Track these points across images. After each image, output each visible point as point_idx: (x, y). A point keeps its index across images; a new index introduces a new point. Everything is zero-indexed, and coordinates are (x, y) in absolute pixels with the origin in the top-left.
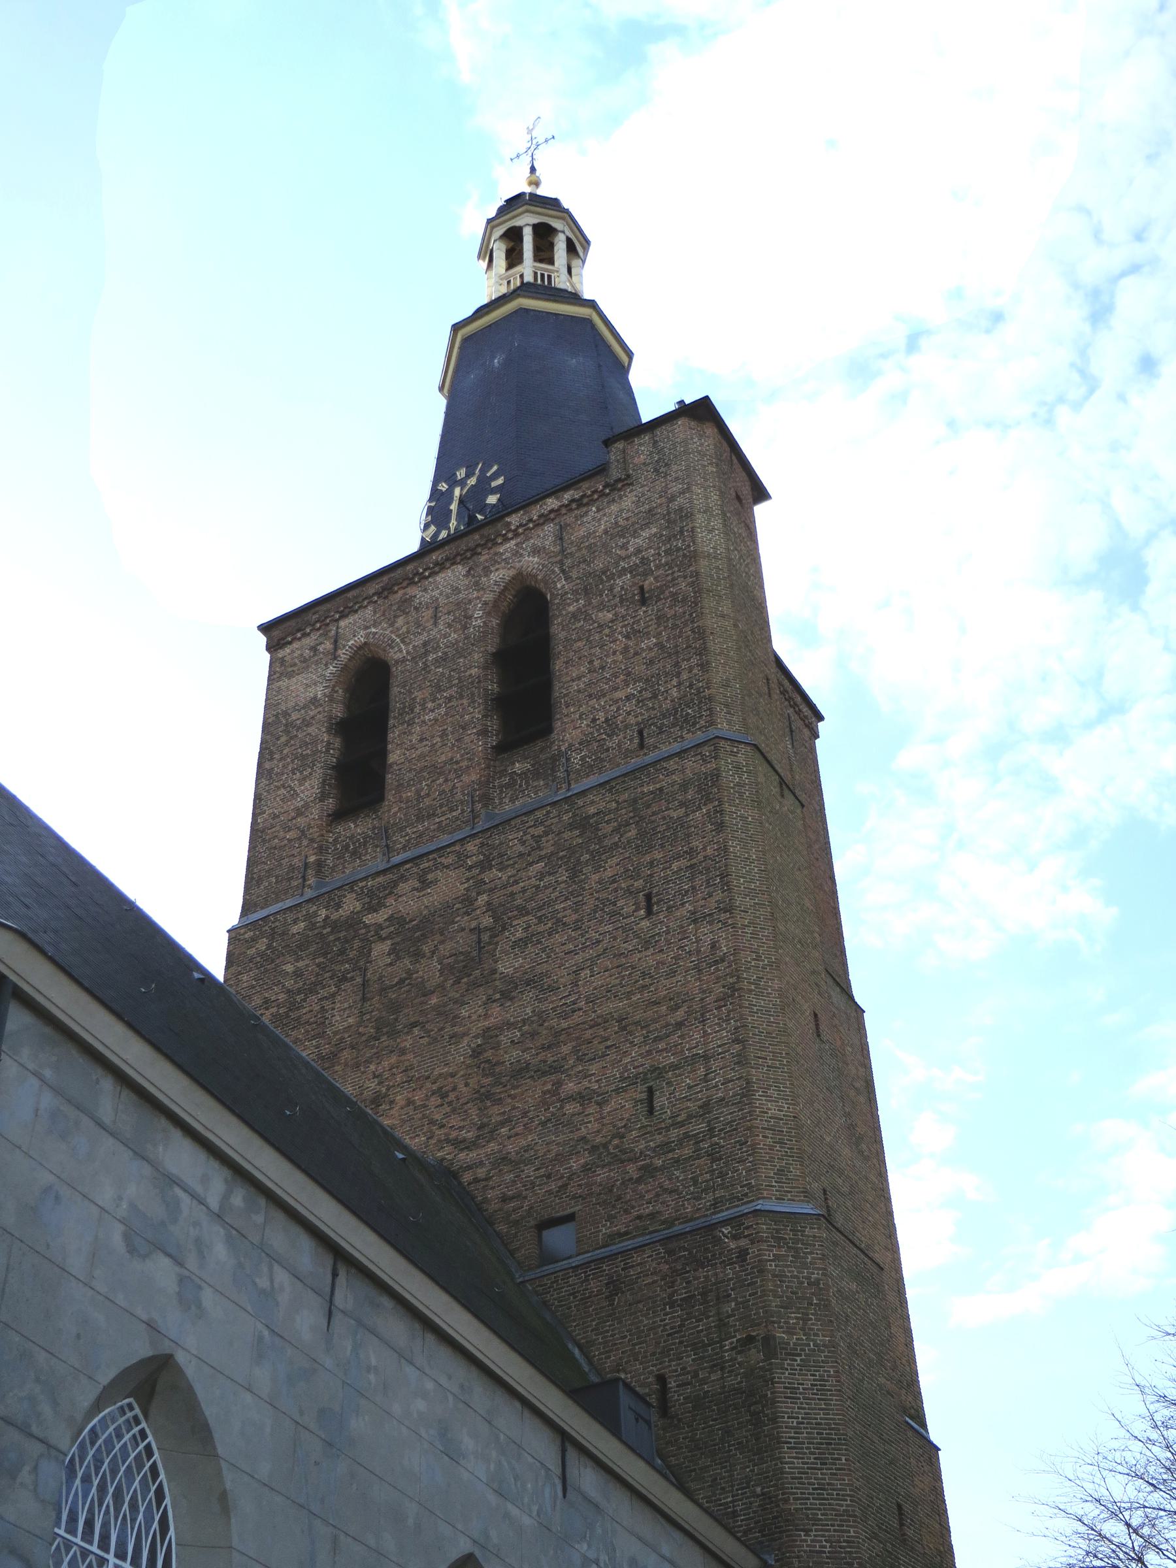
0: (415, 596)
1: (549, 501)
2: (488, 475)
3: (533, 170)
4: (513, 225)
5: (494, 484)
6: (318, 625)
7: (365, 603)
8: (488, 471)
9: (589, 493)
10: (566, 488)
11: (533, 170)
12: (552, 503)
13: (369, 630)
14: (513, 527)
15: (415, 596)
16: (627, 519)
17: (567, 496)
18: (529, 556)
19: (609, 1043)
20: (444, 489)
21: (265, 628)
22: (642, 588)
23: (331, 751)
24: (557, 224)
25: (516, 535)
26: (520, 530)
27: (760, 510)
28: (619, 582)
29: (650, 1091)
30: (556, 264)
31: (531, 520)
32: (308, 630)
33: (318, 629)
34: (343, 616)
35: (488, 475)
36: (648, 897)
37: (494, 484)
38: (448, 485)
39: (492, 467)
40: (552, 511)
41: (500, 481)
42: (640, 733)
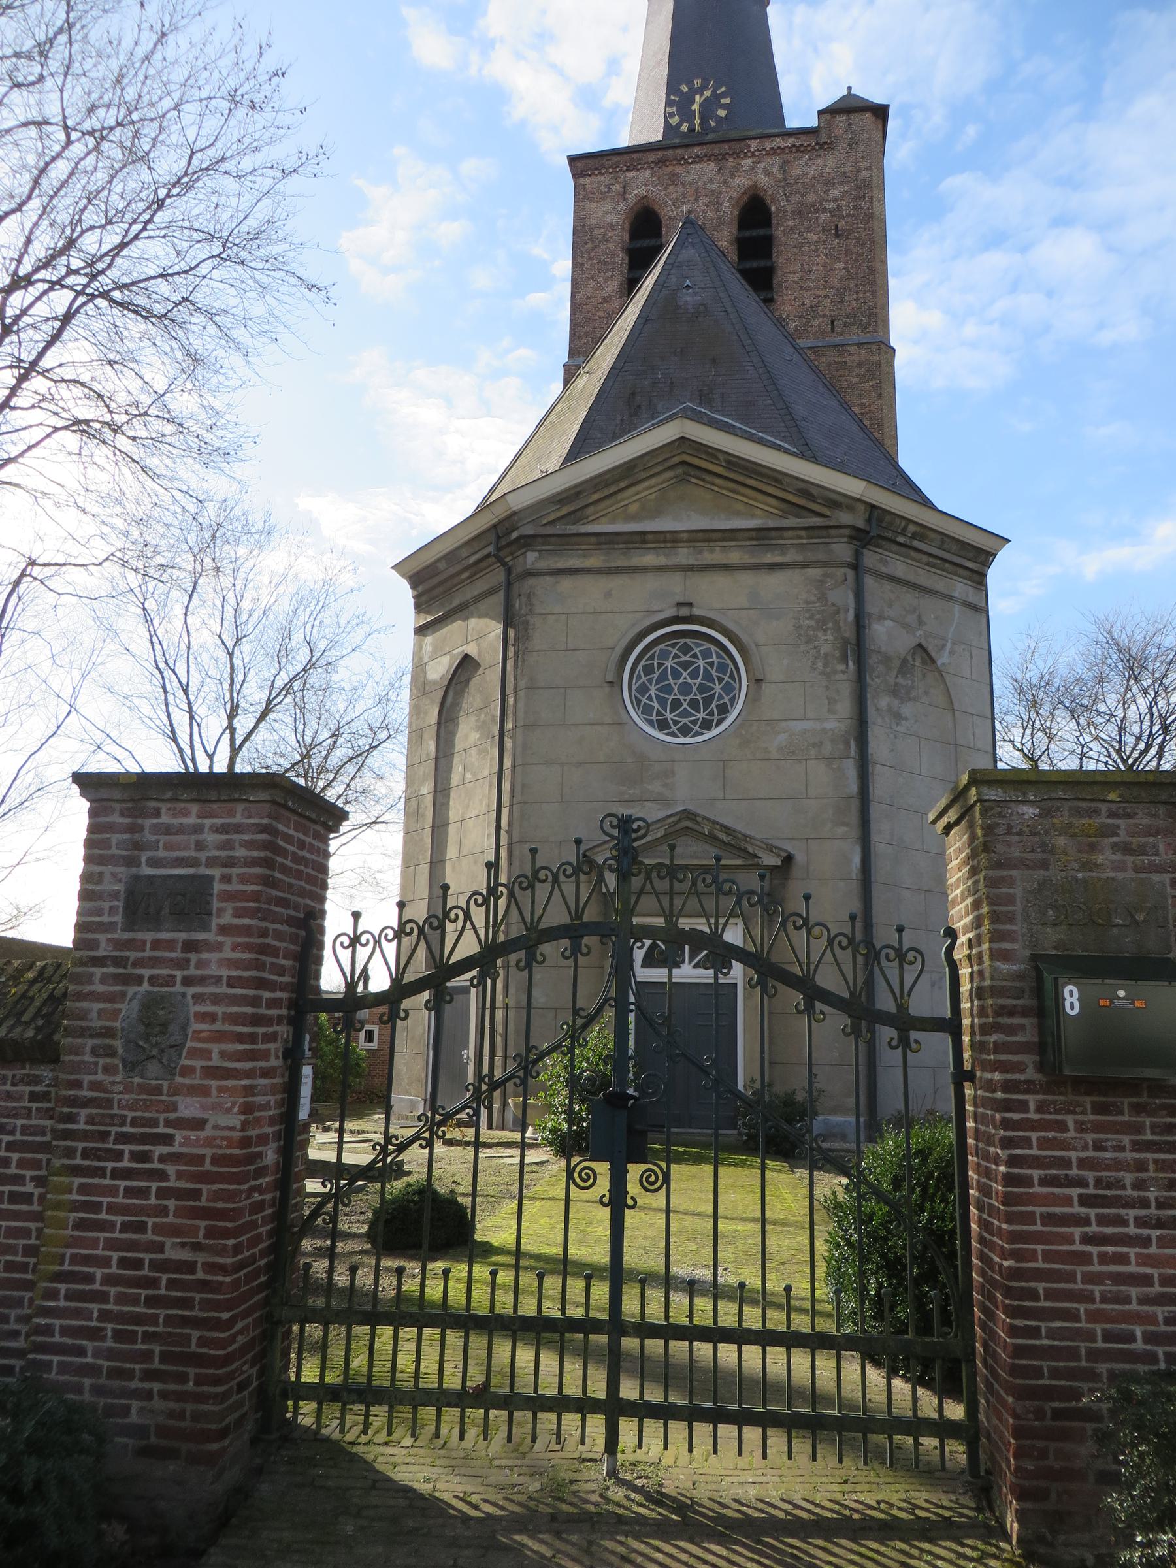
5: (722, 101)
22: (836, 226)
25: (753, 156)
37: (722, 101)
41: (727, 101)
42: (832, 322)
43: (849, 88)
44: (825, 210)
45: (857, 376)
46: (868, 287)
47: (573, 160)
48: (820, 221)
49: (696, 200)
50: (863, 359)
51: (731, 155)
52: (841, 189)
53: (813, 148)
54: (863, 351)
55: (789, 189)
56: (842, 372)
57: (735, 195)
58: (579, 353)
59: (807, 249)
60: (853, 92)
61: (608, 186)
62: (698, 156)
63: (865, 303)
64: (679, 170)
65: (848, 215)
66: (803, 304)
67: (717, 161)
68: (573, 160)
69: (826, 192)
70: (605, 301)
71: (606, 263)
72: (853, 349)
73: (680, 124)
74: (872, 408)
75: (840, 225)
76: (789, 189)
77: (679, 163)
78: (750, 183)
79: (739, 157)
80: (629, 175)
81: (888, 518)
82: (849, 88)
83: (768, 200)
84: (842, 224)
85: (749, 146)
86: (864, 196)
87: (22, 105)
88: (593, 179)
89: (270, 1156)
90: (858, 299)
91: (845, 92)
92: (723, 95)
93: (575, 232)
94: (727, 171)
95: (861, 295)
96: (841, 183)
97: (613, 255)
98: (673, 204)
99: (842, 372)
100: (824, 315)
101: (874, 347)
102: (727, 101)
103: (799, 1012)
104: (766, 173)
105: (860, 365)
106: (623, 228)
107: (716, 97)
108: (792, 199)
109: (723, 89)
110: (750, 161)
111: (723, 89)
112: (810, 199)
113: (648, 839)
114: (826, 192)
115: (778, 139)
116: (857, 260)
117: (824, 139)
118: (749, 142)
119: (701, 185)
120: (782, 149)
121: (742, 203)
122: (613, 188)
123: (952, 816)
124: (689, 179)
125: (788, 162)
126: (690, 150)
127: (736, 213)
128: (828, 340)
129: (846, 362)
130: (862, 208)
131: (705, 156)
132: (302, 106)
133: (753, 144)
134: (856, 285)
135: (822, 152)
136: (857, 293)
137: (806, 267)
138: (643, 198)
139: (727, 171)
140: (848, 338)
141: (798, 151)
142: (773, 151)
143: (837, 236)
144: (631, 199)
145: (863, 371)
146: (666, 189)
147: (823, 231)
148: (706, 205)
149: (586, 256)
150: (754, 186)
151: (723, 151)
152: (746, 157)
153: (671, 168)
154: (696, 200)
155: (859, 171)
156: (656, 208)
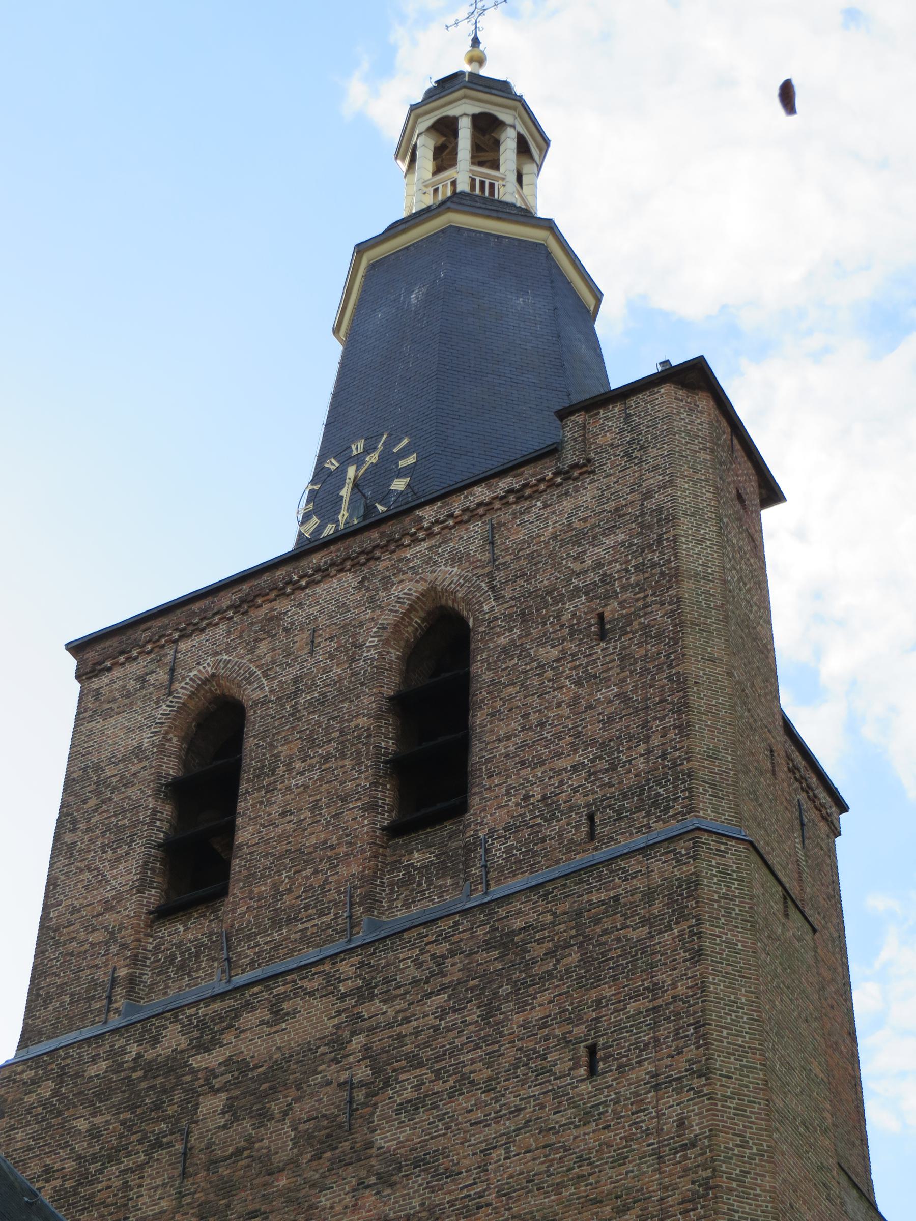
3: (476, 42)
5: (402, 464)
6: (149, 647)
7: (216, 619)
8: (395, 446)
10: (501, 474)
11: (476, 42)
12: (481, 493)
13: (219, 657)
14: (426, 525)
16: (585, 520)
17: (503, 484)
20: (333, 468)
22: (601, 616)
25: (430, 535)
26: (436, 529)
27: (769, 516)
30: (502, 168)
34: (184, 636)
36: (592, 1050)
37: (402, 464)
38: (338, 462)
40: (480, 504)
42: (591, 818)
44: (576, 593)
45: (645, 921)
46: (670, 721)
47: (77, 648)
48: (566, 617)
49: (312, 652)
50: (656, 878)
51: (384, 548)
52: (609, 541)
53: (552, 485)
54: (656, 865)
55: (500, 576)
56: (607, 924)
57: (388, 619)
58: (40, 1033)
59: (536, 681)
61: (142, 680)
62: (318, 570)
63: (664, 756)
64: (282, 605)
65: (624, 588)
66: (526, 798)
67: (356, 565)
68: (77, 648)
69: (578, 558)
70: (108, 907)
71: (119, 829)
72: (632, 865)
74: (681, 989)
75: (608, 615)
76: (500, 576)
77: (282, 594)
78: (422, 587)
79: (401, 546)
80: (183, 646)
83: (462, 608)
84: (612, 609)
85: (421, 519)
86: (659, 541)
88: (117, 673)
90: (648, 752)
92: (404, 453)
93: (69, 784)
94: (377, 581)
95: (656, 741)
96: (611, 530)
97: (135, 809)
98: (265, 674)
99: (607, 924)
100: (571, 809)
101: (682, 847)
104: (456, 559)
105: (649, 896)
106: (162, 751)
107: (389, 458)
108: (508, 593)
111: (405, 441)
112: (543, 581)
113: (501, 1113)
114: (578, 558)
115: (478, 490)
116: (645, 671)
117: (570, 457)
118: (419, 513)
119: (322, 621)
120: (487, 505)
121: (408, 632)
122: (151, 679)
124: (300, 616)
125: (500, 524)
126: (304, 563)
127: (394, 654)
128: (581, 859)
129: (616, 899)
130: (654, 565)
131: (333, 564)
134: (645, 725)
135: (570, 486)
136: (647, 738)
137: (534, 718)
138: (206, 681)
139: (377, 581)
140: (624, 843)
141: (519, 500)
142: (471, 514)
143: (603, 635)
144: (182, 689)
145: (657, 907)
146: (251, 651)
147: (572, 634)
148: (331, 657)
149: (82, 826)
150: (432, 592)
151: (367, 545)
152: (416, 541)
153: (266, 607)
154: (312, 652)
155: (648, 495)
156: (235, 692)
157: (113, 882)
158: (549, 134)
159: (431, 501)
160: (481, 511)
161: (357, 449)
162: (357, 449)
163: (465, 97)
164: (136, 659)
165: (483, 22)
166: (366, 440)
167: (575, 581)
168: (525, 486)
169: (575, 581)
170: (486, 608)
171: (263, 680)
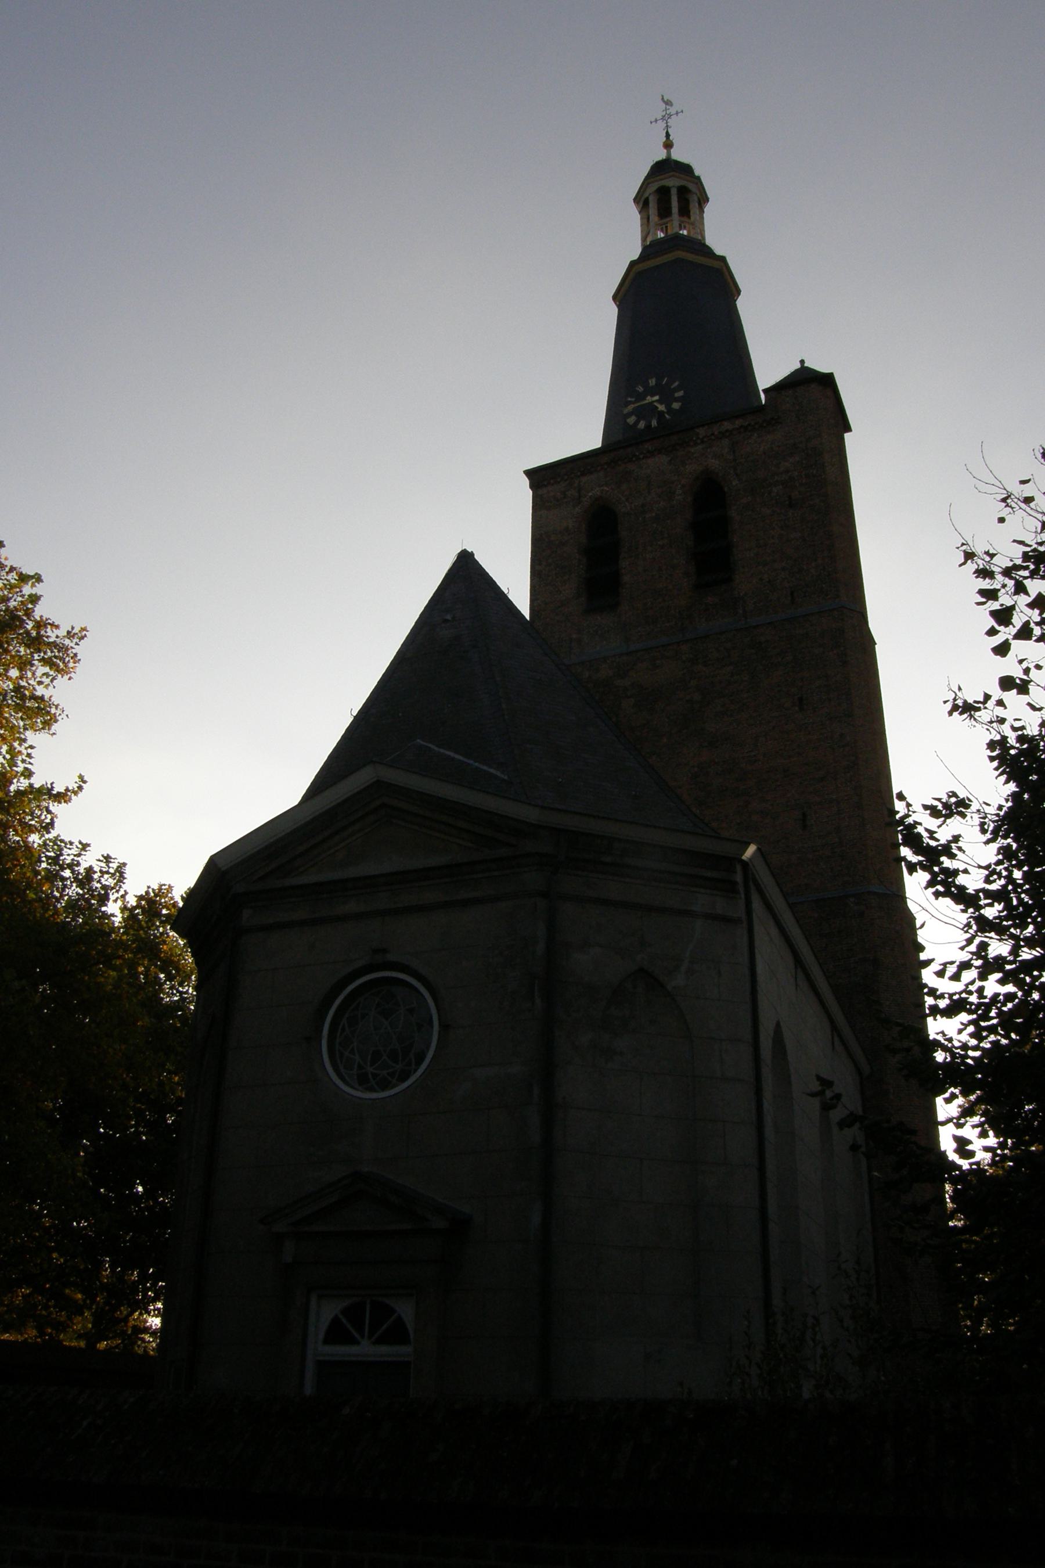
0: (633, 470)
1: (726, 423)
2: (672, 387)
3: (668, 135)
4: (664, 184)
5: (677, 395)
6: (566, 477)
7: (599, 468)
8: (672, 384)
9: (753, 424)
10: (737, 417)
11: (668, 135)
12: (727, 425)
13: (602, 488)
14: (701, 437)
15: (633, 470)
16: (779, 447)
17: (738, 422)
18: (712, 459)
19: (779, 783)
20: (640, 391)
21: (529, 473)
22: (790, 497)
23: (581, 566)
24: (691, 186)
25: (703, 442)
26: (705, 439)
27: (847, 436)
28: (775, 490)
29: (804, 815)
30: (692, 218)
31: (713, 434)
32: (559, 480)
33: (566, 480)
34: (583, 474)
35: (672, 387)
36: (801, 700)
37: (677, 395)
38: (643, 387)
39: (675, 382)
40: (727, 431)
41: (681, 393)
42: (792, 594)
43: (802, 362)
60: (806, 365)
73: (637, 423)
80: (584, 479)
81: (41, 789)
82: (802, 362)
87: (2, 667)
89: (38, 728)
91: (798, 366)
102: (681, 393)
103: (18, 787)
109: (677, 384)
110: (700, 447)
111: (677, 384)
123: (112, 860)
132: (69, 716)
133: (702, 432)
157: (563, 592)
158: (709, 195)
159: (703, 426)
160: (727, 434)
161: (652, 382)
162: (652, 382)
163: (673, 176)
164: (559, 482)
165: (671, 122)
166: (682, 405)
167: (776, 478)
168: (749, 425)
169: (776, 478)
170: (734, 483)
171: (627, 503)
